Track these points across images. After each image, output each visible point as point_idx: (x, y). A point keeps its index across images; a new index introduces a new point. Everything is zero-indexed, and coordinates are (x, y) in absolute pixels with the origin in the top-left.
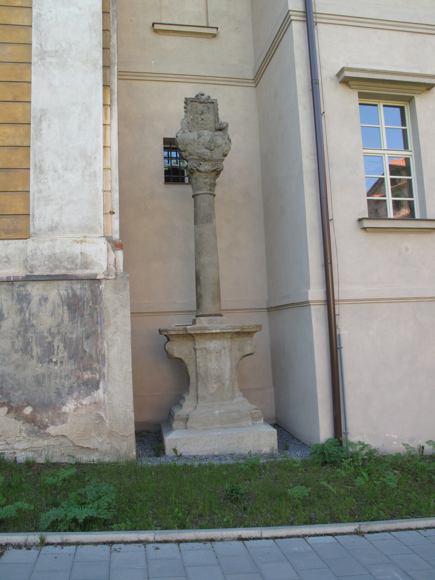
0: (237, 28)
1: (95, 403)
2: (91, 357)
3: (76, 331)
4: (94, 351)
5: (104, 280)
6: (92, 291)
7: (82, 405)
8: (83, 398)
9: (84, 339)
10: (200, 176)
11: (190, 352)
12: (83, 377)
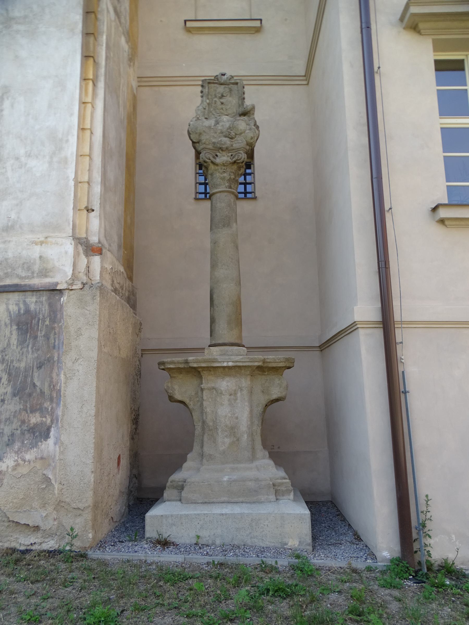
0: (286, 20)
1: (42, 458)
2: (42, 393)
3: (25, 358)
4: (47, 384)
5: (68, 291)
6: (50, 305)
7: (25, 461)
8: (26, 452)
9: (35, 369)
10: (216, 170)
11: (196, 394)
12: (29, 421)
